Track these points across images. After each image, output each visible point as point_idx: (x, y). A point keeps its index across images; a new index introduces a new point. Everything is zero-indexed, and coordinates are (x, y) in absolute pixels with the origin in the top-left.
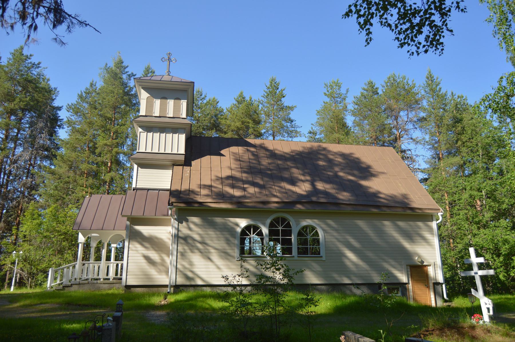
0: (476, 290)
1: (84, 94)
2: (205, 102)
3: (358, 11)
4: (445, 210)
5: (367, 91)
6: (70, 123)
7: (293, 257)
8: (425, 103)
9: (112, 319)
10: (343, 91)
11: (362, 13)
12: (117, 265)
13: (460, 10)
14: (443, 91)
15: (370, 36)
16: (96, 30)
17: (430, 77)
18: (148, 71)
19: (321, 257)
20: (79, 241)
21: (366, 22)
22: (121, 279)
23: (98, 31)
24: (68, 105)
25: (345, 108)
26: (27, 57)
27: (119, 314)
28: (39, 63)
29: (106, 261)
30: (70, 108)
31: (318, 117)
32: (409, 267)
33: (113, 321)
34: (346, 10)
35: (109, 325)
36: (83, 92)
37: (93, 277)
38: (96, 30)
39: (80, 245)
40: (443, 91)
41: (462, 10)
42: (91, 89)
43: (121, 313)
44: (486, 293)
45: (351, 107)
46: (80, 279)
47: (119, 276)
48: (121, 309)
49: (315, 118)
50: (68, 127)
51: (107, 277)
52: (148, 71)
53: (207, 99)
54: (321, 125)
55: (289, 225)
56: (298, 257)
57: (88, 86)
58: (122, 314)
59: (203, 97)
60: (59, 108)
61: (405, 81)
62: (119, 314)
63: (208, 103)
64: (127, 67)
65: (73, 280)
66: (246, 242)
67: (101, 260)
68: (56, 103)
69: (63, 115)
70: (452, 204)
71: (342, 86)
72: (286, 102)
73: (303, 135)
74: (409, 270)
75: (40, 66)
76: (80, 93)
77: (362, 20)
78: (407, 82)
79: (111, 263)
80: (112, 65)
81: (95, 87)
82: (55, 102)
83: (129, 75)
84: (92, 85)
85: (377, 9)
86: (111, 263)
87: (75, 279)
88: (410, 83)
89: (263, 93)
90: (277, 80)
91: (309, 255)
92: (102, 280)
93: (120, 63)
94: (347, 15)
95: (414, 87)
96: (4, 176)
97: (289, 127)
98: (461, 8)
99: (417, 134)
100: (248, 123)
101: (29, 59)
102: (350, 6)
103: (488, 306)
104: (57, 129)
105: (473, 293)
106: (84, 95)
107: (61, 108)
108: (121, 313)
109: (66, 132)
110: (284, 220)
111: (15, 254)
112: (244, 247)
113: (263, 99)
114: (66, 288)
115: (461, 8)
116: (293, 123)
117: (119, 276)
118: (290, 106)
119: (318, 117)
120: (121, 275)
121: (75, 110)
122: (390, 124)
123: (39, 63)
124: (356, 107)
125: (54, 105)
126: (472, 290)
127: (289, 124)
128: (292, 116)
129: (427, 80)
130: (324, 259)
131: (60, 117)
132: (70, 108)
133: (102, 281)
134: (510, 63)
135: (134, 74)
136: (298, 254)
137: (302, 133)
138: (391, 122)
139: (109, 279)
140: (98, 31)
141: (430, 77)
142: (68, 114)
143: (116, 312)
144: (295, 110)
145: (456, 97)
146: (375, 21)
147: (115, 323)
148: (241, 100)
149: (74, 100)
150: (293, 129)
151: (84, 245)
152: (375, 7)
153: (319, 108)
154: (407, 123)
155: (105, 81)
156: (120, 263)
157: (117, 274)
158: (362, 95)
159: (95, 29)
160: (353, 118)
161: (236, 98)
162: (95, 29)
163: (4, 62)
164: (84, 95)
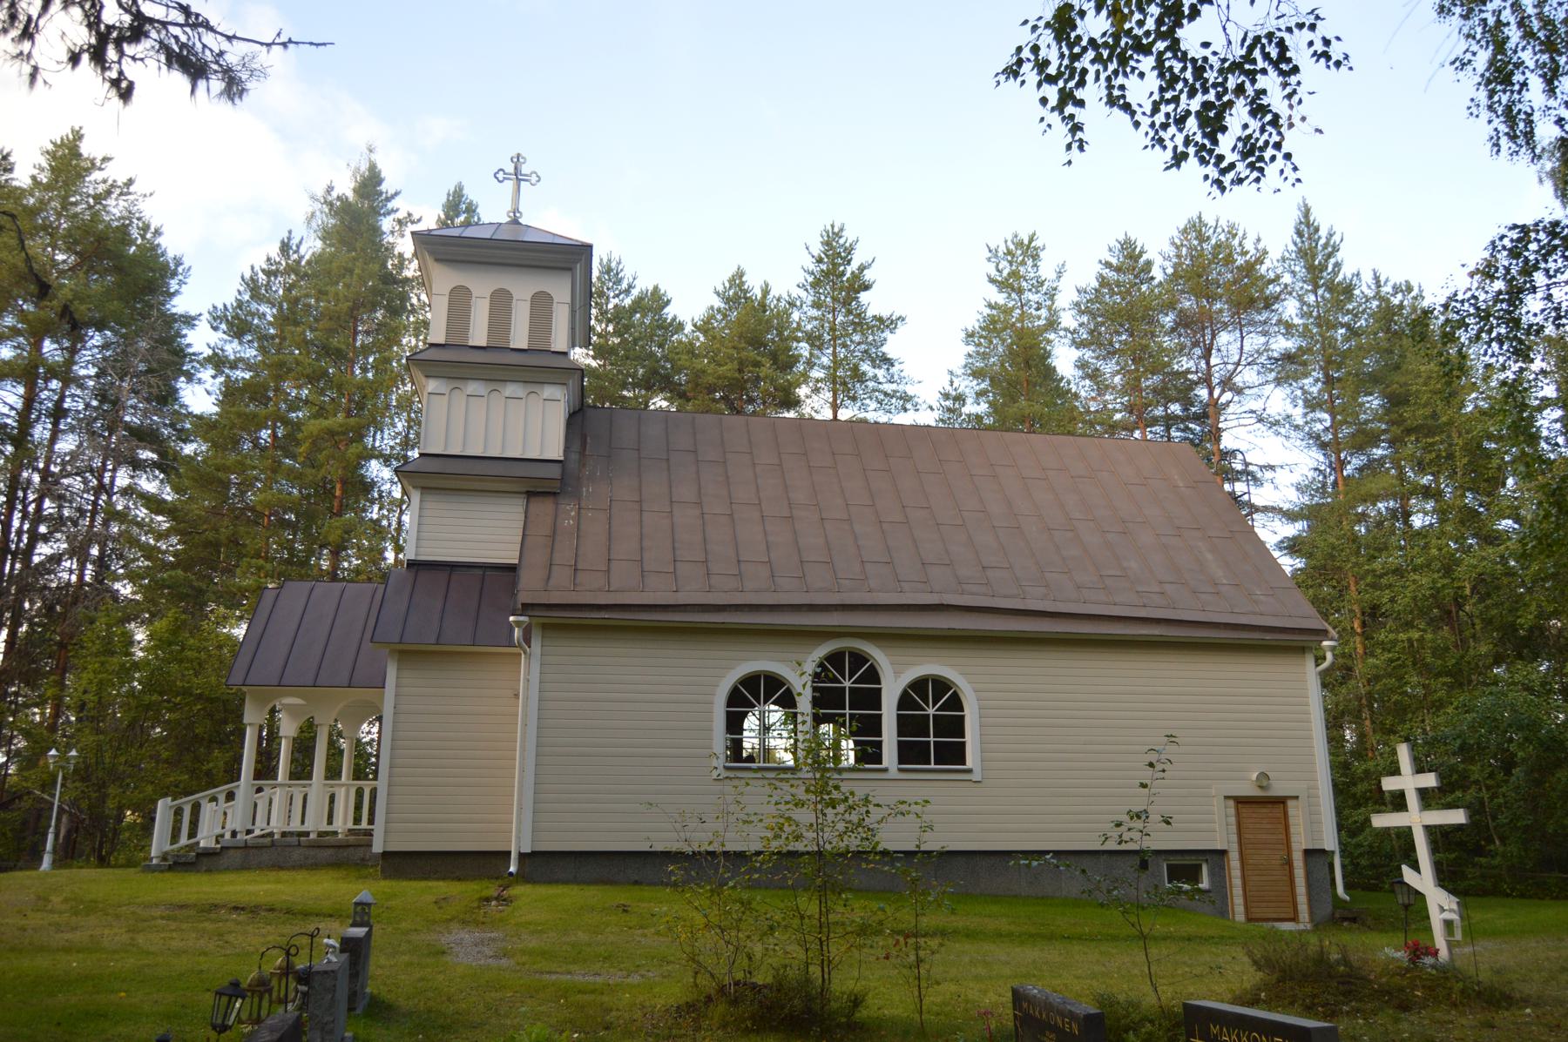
0: (1415, 866)
1: (261, 275)
2: (628, 302)
3: (1042, 65)
4: (1345, 634)
5: (1118, 269)
6: (218, 361)
7: (885, 770)
8: (1290, 309)
9: (337, 945)
10: (1046, 270)
11: (1052, 70)
12: (360, 793)
13: (1331, 63)
14: (1346, 272)
15: (1079, 135)
16: (318, 45)
17: (1306, 227)
18: (456, 204)
19: (969, 771)
20: (246, 720)
21: (1066, 97)
22: (369, 833)
23: (324, 44)
24: (215, 307)
25: (1052, 324)
26: (93, 164)
27: (360, 932)
28: (130, 182)
29: (327, 778)
30: (217, 318)
31: (971, 349)
32: (1231, 803)
33: (342, 951)
34: (1007, 59)
35: (329, 962)
36: (257, 268)
37: (287, 829)
38: (318, 45)
39: (248, 730)
40: (1346, 272)
41: (1338, 64)
42: (284, 263)
43: (366, 929)
44: (1447, 877)
45: (1068, 320)
46: (249, 832)
47: (364, 825)
48: (366, 918)
49: (958, 354)
50: (214, 377)
51: (330, 828)
52: (456, 204)
53: (635, 292)
54: (977, 374)
55: (873, 675)
56: (900, 770)
57: (274, 251)
58: (369, 934)
59: (624, 285)
60: (189, 321)
61: (1236, 242)
62: (360, 932)
63: (638, 304)
64: (397, 194)
65: (228, 836)
66: (746, 725)
67: (311, 779)
68: (179, 306)
69: (201, 339)
70: (1373, 614)
71: (1042, 254)
72: (873, 303)
73: (925, 406)
74: (1232, 811)
75: (132, 189)
76: (248, 275)
77: (1052, 93)
78: (1240, 244)
79: (343, 785)
80: (345, 187)
81: (296, 256)
82: (176, 301)
83: (400, 222)
84: (285, 247)
85: (1097, 59)
86: (343, 785)
87: (234, 834)
88: (1249, 245)
89: (801, 277)
90: (849, 236)
91: (932, 766)
92: (313, 836)
93: (370, 184)
94: (1013, 71)
95: (1260, 261)
96: (22, 524)
97: (881, 380)
98: (1334, 59)
99: (1279, 401)
100: (757, 364)
101: (100, 169)
102: (1019, 49)
103: (1447, 916)
104: (181, 383)
105: (1407, 879)
106: (262, 277)
107: (194, 318)
108: (366, 929)
109: (208, 393)
110: (859, 659)
111: (53, 756)
112: (741, 741)
113: (803, 294)
114: (205, 860)
115: (1334, 59)
116: (893, 370)
117: (364, 825)
118: (885, 314)
119: (971, 349)
120: (371, 822)
121: (237, 324)
122: (1188, 371)
123: (130, 182)
124: (1085, 319)
125: (174, 310)
126: (1405, 868)
127: (881, 373)
128: (890, 349)
129: (1295, 236)
130: (976, 776)
131: (189, 345)
132: (217, 318)
133: (314, 840)
134: (1549, 186)
135: (416, 217)
136: (900, 763)
137: (920, 401)
138: (1191, 365)
139: (336, 833)
140: (324, 44)
141: (1306, 227)
142: (216, 338)
143: (354, 925)
144: (901, 328)
145: (1388, 289)
146: (1093, 92)
147: (345, 956)
148: (736, 293)
149: (227, 293)
150: (894, 387)
151: (261, 731)
152: (1091, 54)
153: (973, 322)
154: (1240, 368)
155: (326, 235)
156: (367, 786)
157: (357, 820)
158: (1103, 282)
159: (311, 44)
160: (1075, 354)
161: (720, 289)
162: (311, 44)
163: (21, 177)
164: (262, 277)
